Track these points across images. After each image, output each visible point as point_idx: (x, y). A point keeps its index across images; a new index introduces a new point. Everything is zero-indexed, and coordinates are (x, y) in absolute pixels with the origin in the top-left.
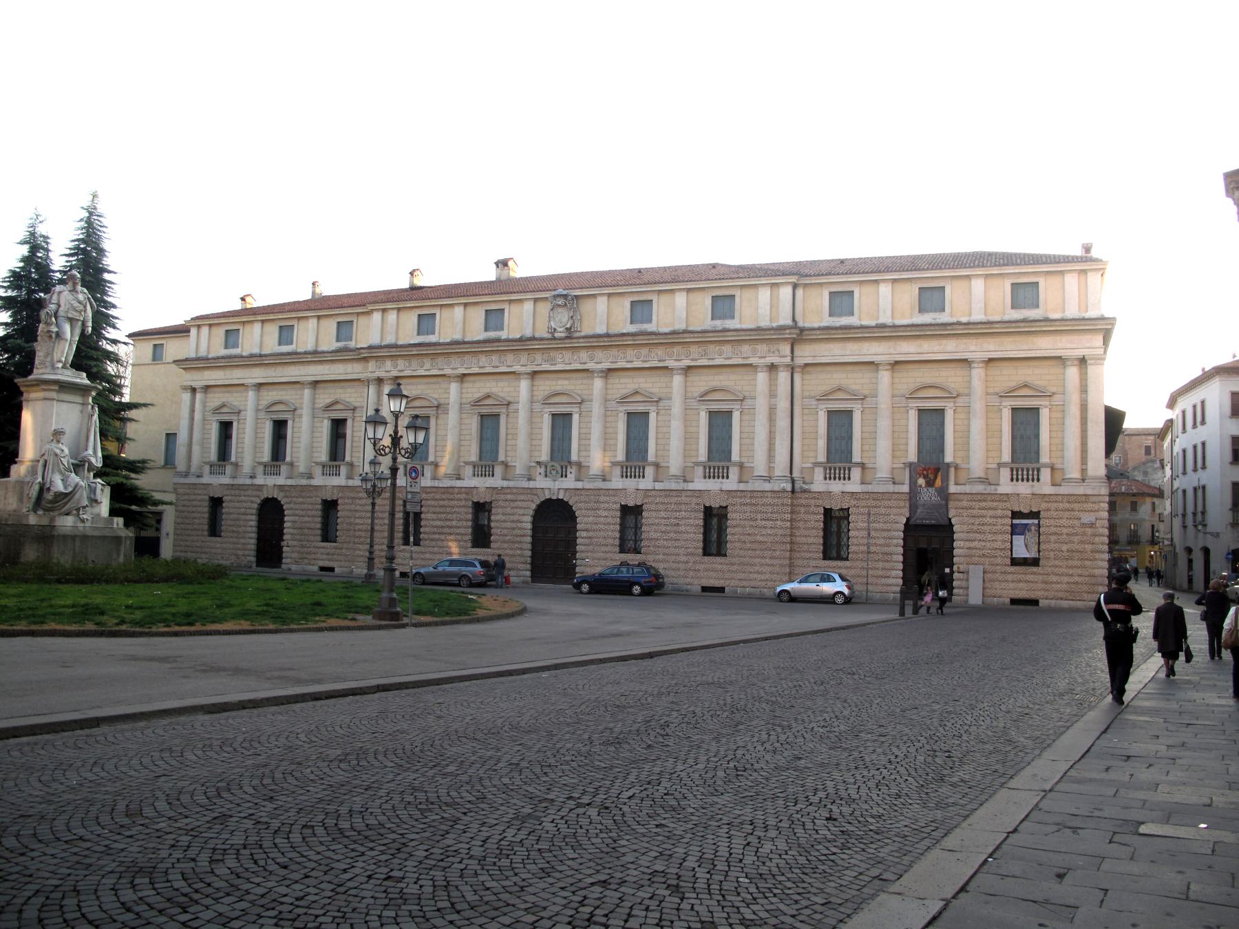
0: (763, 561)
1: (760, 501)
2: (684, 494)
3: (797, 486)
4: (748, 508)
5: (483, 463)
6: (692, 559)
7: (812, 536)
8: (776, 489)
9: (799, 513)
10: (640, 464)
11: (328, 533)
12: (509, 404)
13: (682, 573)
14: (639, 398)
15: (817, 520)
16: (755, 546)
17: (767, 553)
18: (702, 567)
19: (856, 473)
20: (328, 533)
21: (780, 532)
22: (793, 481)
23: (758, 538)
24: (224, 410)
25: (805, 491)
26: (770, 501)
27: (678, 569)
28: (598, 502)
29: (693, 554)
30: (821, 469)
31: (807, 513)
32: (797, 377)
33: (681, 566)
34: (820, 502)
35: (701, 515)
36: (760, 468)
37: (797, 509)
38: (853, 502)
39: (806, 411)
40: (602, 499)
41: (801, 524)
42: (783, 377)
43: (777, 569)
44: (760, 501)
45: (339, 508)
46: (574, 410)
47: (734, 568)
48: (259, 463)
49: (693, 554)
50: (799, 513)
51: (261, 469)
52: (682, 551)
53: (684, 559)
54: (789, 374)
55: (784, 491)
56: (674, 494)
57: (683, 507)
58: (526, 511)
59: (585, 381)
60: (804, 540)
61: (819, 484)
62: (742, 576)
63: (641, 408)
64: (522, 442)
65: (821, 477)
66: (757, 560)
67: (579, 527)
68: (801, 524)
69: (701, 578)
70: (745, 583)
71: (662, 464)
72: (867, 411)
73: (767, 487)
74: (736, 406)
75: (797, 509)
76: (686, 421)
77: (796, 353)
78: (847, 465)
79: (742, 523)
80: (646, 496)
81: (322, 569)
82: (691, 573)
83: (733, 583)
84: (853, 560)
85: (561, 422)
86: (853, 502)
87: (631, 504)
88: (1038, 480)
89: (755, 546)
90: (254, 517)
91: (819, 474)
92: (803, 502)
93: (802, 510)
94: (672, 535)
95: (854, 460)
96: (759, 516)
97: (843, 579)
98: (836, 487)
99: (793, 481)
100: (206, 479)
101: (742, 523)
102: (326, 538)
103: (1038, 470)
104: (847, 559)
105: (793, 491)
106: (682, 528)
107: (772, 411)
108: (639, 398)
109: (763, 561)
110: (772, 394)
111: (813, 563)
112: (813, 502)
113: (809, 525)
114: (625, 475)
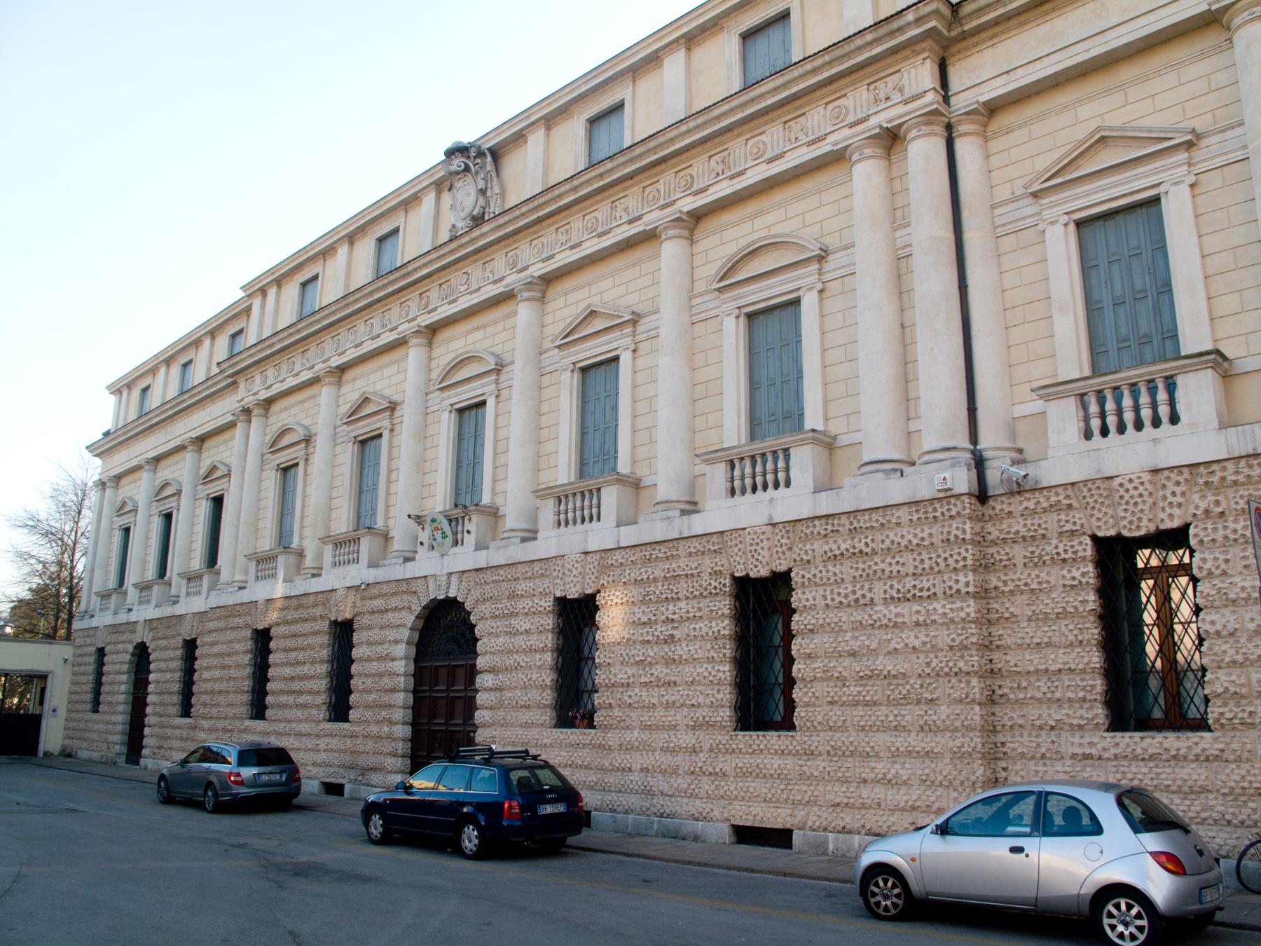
0: (900, 742)
1: (881, 540)
2: (683, 549)
3: (993, 476)
4: (845, 570)
5: (759, 446)
6: (707, 739)
7: (1062, 644)
8: (924, 492)
9: (1009, 566)
10: (1158, 370)
11: (762, 695)
12: (635, 321)
13: (682, 782)
14: (599, 324)
15: (1075, 588)
16: (875, 691)
17: (911, 714)
18: (726, 764)
19: (1198, 393)
20: (762, 695)
21: (944, 637)
22: (979, 463)
23: (885, 664)
24: (285, 441)
25: (1019, 489)
26: (909, 535)
27: (674, 772)
28: (513, 596)
29: (708, 725)
30: (1071, 405)
31: (1036, 562)
32: (966, 150)
33: (681, 760)
34: (1079, 517)
35: (1087, 572)
36: (876, 435)
37: (999, 553)
38: (1200, 502)
39: (1007, 243)
40: (522, 587)
41: (1018, 606)
42: (924, 152)
43: (944, 767)
44: (881, 540)
45: (796, 599)
46: (1171, 182)
47: (818, 765)
48: (709, 457)
49: (708, 725)
50: (1009, 566)
51: (718, 475)
52: (682, 717)
53: (687, 739)
54: (939, 145)
55: (948, 496)
56: (660, 552)
57: (682, 587)
58: (391, 634)
59: (828, 197)
60: (1032, 660)
61: (1065, 454)
62: (838, 793)
63: (774, 290)
64: (517, 456)
65: (1073, 429)
66: (881, 740)
67: (481, 662)
68: (1018, 606)
69: (729, 798)
70: (848, 819)
71: (646, 481)
72: (1211, 182)
73: (896, 490)
74: (806, 277)
75: (999, 553)
76: (692, 354)
77: (955, 83)
78: (1158, 370)
79: (832, 616)
80: (605, 568)
81: (746, 835)
82: (706, 785)
83: (817, 816)
84: (1228, 726)
85: (771, 325)
86: (1200, 502)
87: (573, 594)
88: (1174, 419)
89: (875, 691)
90: (124, 677)
91: (1064, 419)
92: (1018, 525)
93: (1019, 553)
94: (660, 670)
95: (1187, 347)
96: (879, 590)
97: (1147, 815)
98: (1129, 455)
99: (979, 463)
100: (550, 542)
101: (832, 616)
102: (186, 711)
103: (1171, 388)
104: (1202, 725)
105: (982, 496)
106: (681, 650)
107: (900, 261)
108: (599, 324)
109: (900, 742)
110: (897, 217)
111: (1072, 743)
112: (1051, 522)
113: (1047, 604)
114: (1099, 427)
